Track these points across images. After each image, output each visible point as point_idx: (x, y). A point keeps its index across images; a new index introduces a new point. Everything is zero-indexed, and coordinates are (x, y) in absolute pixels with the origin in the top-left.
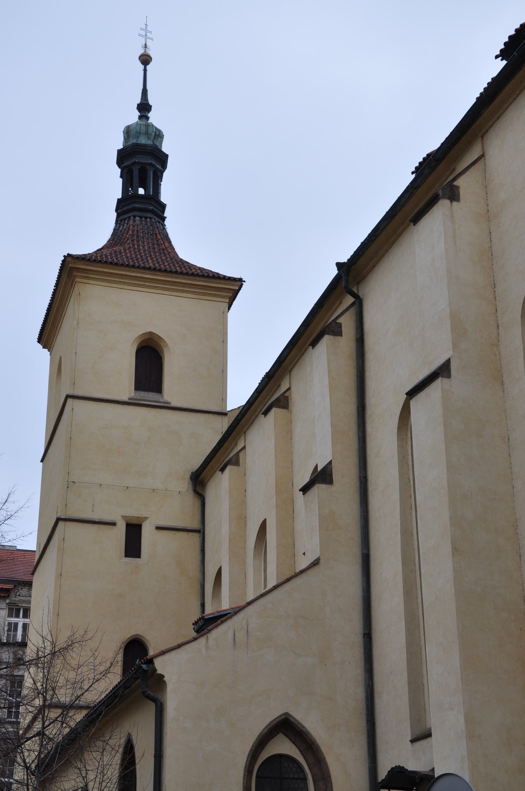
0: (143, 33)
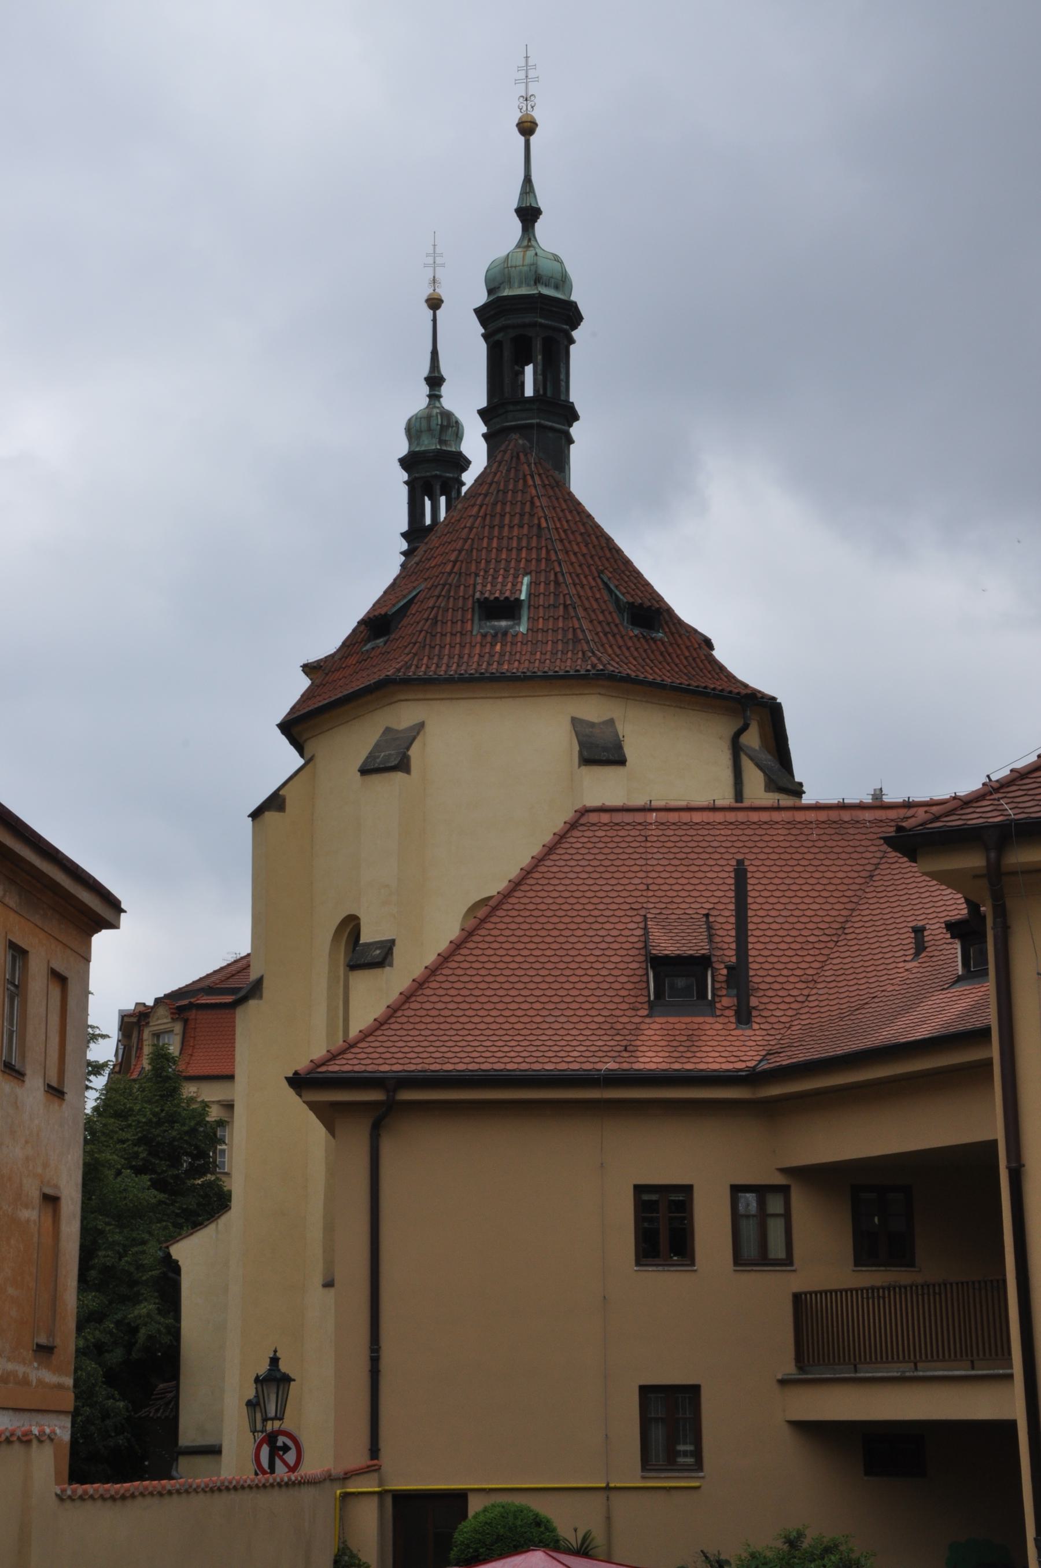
0: (430, 260)
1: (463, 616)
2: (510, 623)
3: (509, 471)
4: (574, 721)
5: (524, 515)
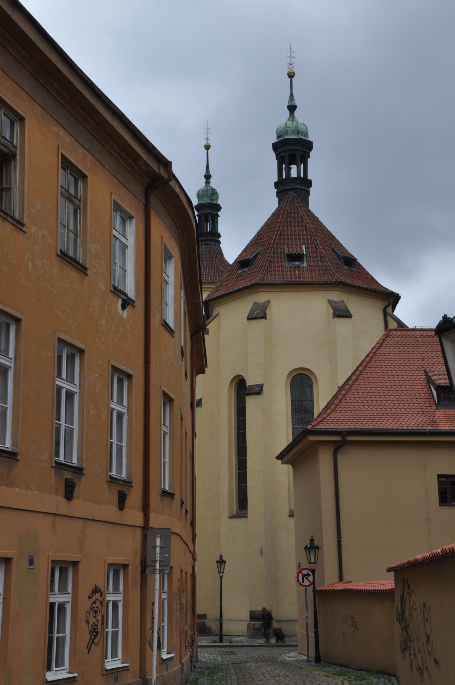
0: (206, 131)
1: (281, 260)
2: (300, 263)
3: (291, 205)
4: (329, 301)
5: (299, 222)
